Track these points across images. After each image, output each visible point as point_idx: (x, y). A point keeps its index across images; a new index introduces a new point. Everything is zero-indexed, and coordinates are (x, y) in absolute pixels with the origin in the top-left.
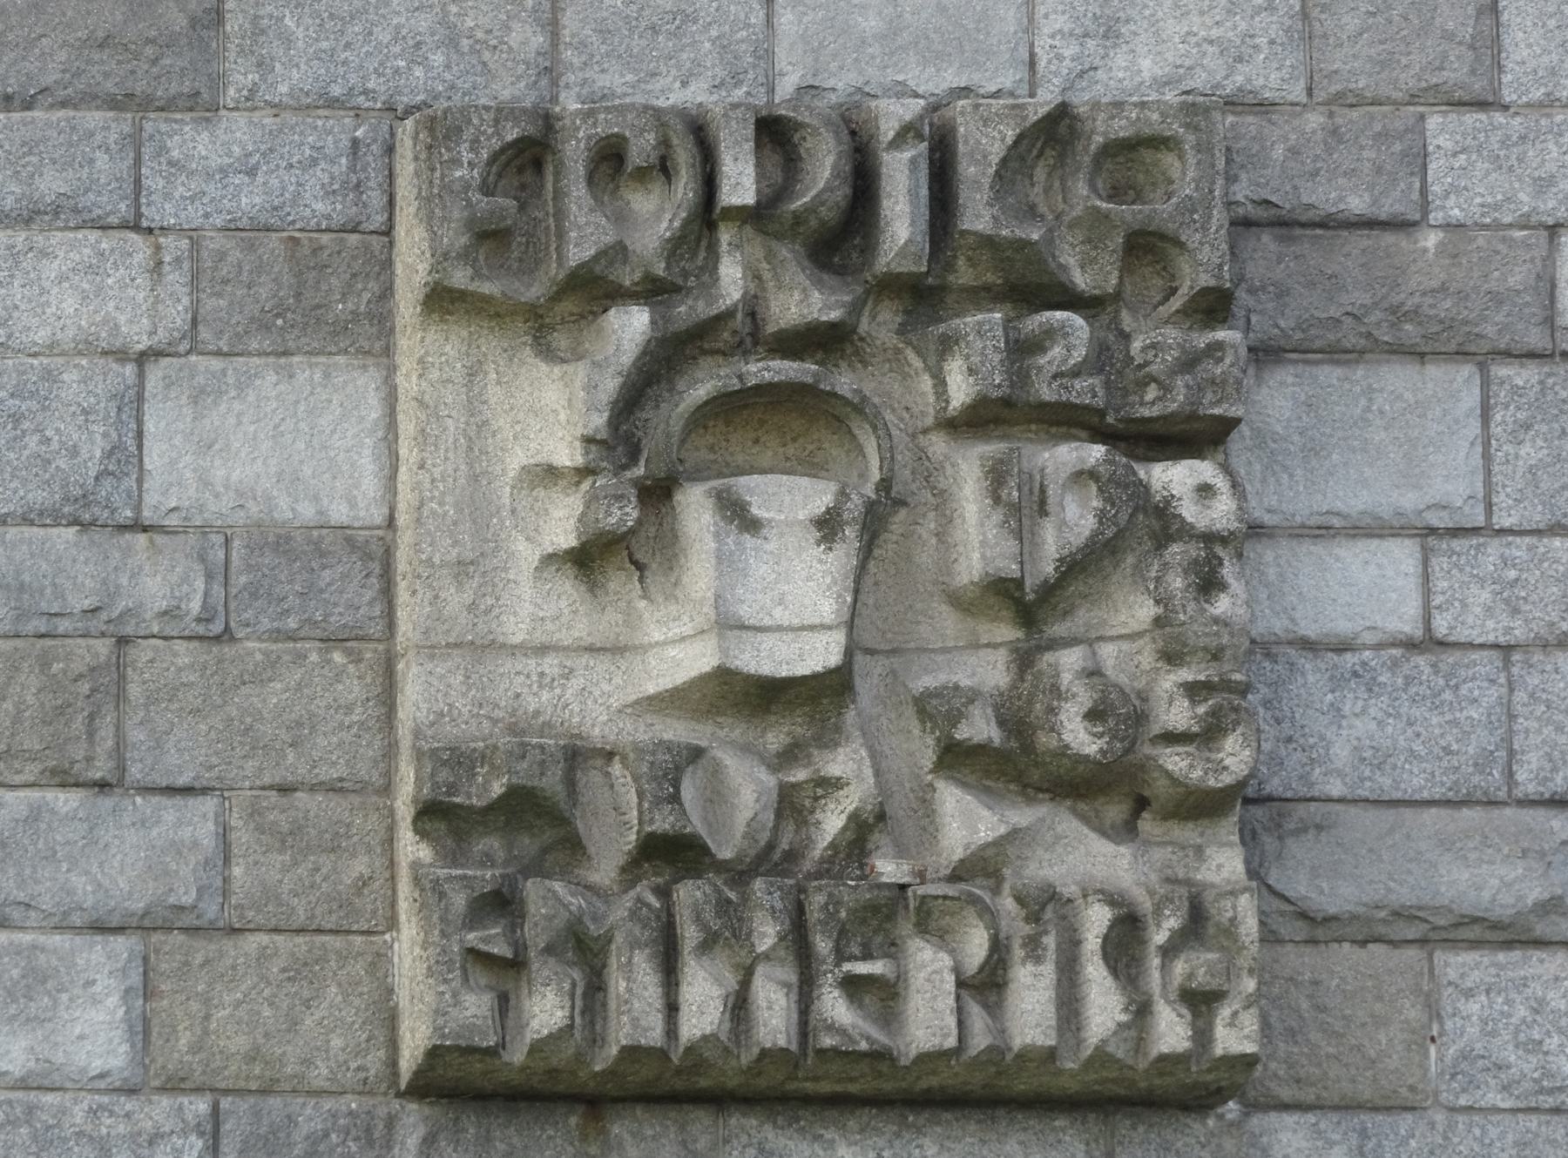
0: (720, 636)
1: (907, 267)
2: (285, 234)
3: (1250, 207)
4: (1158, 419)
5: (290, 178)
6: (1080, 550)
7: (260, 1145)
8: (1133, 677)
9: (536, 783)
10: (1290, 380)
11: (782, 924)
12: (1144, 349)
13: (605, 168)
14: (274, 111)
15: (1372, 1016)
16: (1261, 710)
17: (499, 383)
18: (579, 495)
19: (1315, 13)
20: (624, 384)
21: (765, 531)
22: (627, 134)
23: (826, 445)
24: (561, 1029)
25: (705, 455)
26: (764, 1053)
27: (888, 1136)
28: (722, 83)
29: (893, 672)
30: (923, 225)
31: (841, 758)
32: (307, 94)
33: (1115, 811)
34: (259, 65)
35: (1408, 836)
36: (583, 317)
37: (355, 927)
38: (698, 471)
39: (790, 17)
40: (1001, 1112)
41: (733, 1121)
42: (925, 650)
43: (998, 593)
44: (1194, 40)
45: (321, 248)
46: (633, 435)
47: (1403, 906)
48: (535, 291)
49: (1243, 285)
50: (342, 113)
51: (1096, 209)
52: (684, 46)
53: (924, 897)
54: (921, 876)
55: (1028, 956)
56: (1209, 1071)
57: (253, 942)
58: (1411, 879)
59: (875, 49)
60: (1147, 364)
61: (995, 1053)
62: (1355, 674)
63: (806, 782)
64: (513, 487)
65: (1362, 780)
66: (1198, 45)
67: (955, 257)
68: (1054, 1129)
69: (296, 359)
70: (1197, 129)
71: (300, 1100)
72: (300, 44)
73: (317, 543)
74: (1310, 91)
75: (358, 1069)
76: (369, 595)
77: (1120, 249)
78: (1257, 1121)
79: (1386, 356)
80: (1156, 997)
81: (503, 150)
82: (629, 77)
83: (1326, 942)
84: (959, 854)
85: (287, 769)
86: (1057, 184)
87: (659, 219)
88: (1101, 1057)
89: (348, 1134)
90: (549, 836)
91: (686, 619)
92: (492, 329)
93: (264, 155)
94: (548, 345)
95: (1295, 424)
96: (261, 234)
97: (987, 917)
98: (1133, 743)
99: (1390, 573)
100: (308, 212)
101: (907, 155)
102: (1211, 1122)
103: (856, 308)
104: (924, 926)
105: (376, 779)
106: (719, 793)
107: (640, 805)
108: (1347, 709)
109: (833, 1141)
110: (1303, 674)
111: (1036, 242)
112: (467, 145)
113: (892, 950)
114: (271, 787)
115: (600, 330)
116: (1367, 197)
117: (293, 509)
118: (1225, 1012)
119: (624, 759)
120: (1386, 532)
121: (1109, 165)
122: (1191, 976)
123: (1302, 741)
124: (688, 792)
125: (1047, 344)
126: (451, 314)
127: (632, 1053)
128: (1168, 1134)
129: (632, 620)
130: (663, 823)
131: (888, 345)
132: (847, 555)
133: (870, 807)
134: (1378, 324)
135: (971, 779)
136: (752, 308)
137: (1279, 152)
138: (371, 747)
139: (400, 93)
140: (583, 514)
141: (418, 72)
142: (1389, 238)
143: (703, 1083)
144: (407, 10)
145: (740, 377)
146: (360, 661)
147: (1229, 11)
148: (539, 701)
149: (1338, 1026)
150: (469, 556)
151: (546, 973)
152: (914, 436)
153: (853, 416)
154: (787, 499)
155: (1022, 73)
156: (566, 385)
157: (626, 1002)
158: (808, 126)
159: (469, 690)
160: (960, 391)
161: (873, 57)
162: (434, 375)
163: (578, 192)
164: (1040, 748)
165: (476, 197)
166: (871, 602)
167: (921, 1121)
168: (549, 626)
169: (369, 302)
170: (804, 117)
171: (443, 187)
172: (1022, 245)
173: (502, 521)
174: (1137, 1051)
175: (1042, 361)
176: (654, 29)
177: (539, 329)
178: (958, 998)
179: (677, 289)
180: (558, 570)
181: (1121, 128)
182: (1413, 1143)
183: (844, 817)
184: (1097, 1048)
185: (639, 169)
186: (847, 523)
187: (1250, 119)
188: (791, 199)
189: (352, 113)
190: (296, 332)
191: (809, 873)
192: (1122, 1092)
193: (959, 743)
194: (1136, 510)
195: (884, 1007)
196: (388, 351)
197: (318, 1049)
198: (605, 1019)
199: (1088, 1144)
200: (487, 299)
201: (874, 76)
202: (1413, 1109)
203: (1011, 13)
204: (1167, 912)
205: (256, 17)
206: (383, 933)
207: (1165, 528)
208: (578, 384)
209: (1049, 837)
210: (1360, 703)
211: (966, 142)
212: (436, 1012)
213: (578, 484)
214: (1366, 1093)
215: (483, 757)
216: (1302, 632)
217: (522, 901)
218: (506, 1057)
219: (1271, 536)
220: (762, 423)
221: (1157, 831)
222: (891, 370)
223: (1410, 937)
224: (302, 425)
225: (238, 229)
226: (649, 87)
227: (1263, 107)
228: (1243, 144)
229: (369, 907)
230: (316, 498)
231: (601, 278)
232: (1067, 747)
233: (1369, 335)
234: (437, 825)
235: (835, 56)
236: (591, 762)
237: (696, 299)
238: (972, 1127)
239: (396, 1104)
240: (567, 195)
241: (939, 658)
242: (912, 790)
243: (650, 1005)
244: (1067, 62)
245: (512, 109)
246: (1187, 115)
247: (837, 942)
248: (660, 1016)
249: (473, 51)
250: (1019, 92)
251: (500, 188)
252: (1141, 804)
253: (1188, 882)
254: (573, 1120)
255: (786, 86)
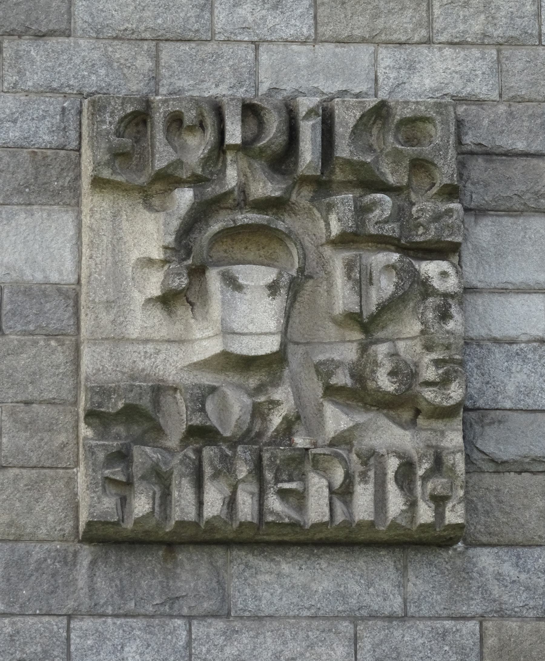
0: (224, 337)
1: (311, 173)
2: (30, 150)
3: (473, 146)
4: (423, 242)
5: (33, 125)
6: (387, 300)
7: (14, 564)
8: (413, 356)
9: (138, 403)
10: (490, 223)
11: (250, 466)
12: (417, 211)
13: (174, 125)
14: (26, 93)
15: (523, 505)
16: (475, 370)
17: (127, 220)
18: (163, 272)
19: (503, 60)
20: (182, 223)
21: (245, 290)
22: (183, 111)
23: (277, 251)
24: (148, 514)
25: (222, 254)
26: (241, 524)
27: (304, 559)
28: (234, 86)
29: (307, 353)
30: (318, 154)
31: (280, 391)
32: (41, 86)
33: (407, 415)
34: (19, 72)
35: (539, 426)
36: (166, 191)
37: (60, 466)
38: (219, 261)
39: (266, 56)
40: (356, 548)
41: (234, 553)
42: (321, 343)
43: (351, 319)
44: (449, 71)
45: (47, 157)
46: (189, 245)
47: (536, 457)
48: (143, 180)
49: (469, 181)
50: (58, 95)
51: (397, 149)
52: (217, 68)
53: (315, 454)
54: (315, 445)
55: (361, 481)
56: (444, 530)
57: (12, 472)
58: (540, 445)
59: (305, 72)
60: (419, 218)
61: (347, 524)
62: (517, 354)
63: (265, 402)
64: (133, 268)
65: (520, 401)
66: (451, 74)
67: (334, 168)
68: (380, 556)
69: (35, 207)
70: (441, 114)
71: (33, 544)
72: (38, 63)
73: (44, 291)
74: (500, 95)
75: (60, 530)
76: (67, 315)
77: (408, 166)
78: (471, 552)
79: (533, 214)
80: (419, 499)
81: (126, 116)
82: (192, 82)
83: (503, 472)
84: (332, 435)
85: (28, 394)
86: (381, 136)
87: (199, 149)
88: (394, 525)
89: (55, 559)
90: (146, 425)
91: (210, 328)
92: (124, 196)
93: (20, 113)
94: (150, 204)
95: (492, 243)
96: (19, 150)
97: (343, 463)
98: (410, 386)
99: (533, 310)
100: (41, 140)
101: (311, 123)
102: (450, 552)
103: (289, 191)
104: (316, 466)
105: (70, 398)
106: (225, 406)
107: (187, 412)
108: (514, 369)
109: (280, 561)
110: (494, 354)
111: (369, 163)
112: (109, 114)
113: (303, 477)
114: (21, 402)
115: (172, 198)
116: (525, 143)
117: (32, 275)
118: (450, 505)
119: (181, 391)
120: (532, 291)
121: (403, 128)
122: (434, 489)
123: (493, 383)
124: (210, 406)
125: (374, 208)
126: (105, 189)
127: (181, 524)
128: (431, 557)
129: (187, 328)
130: (197, 420)
131: (306, 206)
132: (282, 301)
133: (292, 414)
134: (529, 199)
135: (341, 401)
136: (243, 189)
137: (486, 122)
138: (68, 384)
139: (85, 87)
140: (164, 281)
141: (93, 77)
142: (535, 161)
143: (218, 536)
144: (89, 49)
145: (234, 221)
146: (63, 345)
147: (464, 59)
148: (144, 364)
149: (508, 509)
150: (113, 298)
151: (141, 488)
152: (317, 247)
153: (286, 239)
154: (256, 276)
155: (371, 84)
156: (157, 223)
157: (178, 501)
158: (266, 109)
159: (112, 358)
160: (335, 229)
161: (303, 76)
162: (97, 216)
163: (160, 136)
164: (369, 388)
165: (112, 138)
166: (297, 321)
167: (320, 552)
168: (150, 331)
169: (69, 182)
170: (265, 105)
171: (97, 133)
172: (363, 164)
173: (128, 283)
174: (412, 522)
175: (371, 216)
176: (203, 61)
177: (146, 196)
178: (331, 499)
179: (208, 180)
180: (153, 305)
181: (408, 113)
182: (540, 561)
183: (281, 418)
184: (392, 521)
185: (189, 126)
186: (282, 287)
187: (473, 107)
188: (259, 142)
189: (62, 95)
190: (35, 194)
191: (266, 443)
192: (408, 539)
193: (332, 386)
194: (413, 283)
195: (299, 503)
196: (78, 204)
197: (42, 521)
198: (171, 508)
199: (395, 562)
200: (118, 183)
201: (304, 84)
202: (541, 546)
203: (367, 57)
204: (424, 461)
205: (17, 50)
206: (73, 468)
207: (426, 291)
208: (161, 222)
209: (374, 427)
210: (519, 367)
211: (339, 117)
212: (90, 506)
213: (163, 267)
214: (520, 538)
215: (115, 390)
216: (494, 335)
217: (132, 456)
218: (124, 526)
219: (481, 292)
220: (248, 240)
221: (426, 424)
222: (307, 217)
223: (540, 470)
224: (37, 237)
225: (8, 147)
226: (200, 87)
227: (480, 102)
228: (470, 118)
229: (67, 457)
230: (44, 271)
231: (172, 175)
232: (380, 388)
233: (525, 204)
234: (95, 420)
235: (286, 75)
236: (167, 392)
237: (216, 185)
238: (343, 555)
239: (78, 546)
240: (155, 137)
241: (327, 347)
242: (315, 406)
243: (189, 502)
244: (392, 80)
245: (130, 98)
246: (437, 108)
247: (276, 474)
248: (194, 507)
249: (119, 68)
250: (369, 93)
251: (126, 134)
252: (418, 412)
253: (437, 447)
254: (161, 553)
255: (264, 88)
